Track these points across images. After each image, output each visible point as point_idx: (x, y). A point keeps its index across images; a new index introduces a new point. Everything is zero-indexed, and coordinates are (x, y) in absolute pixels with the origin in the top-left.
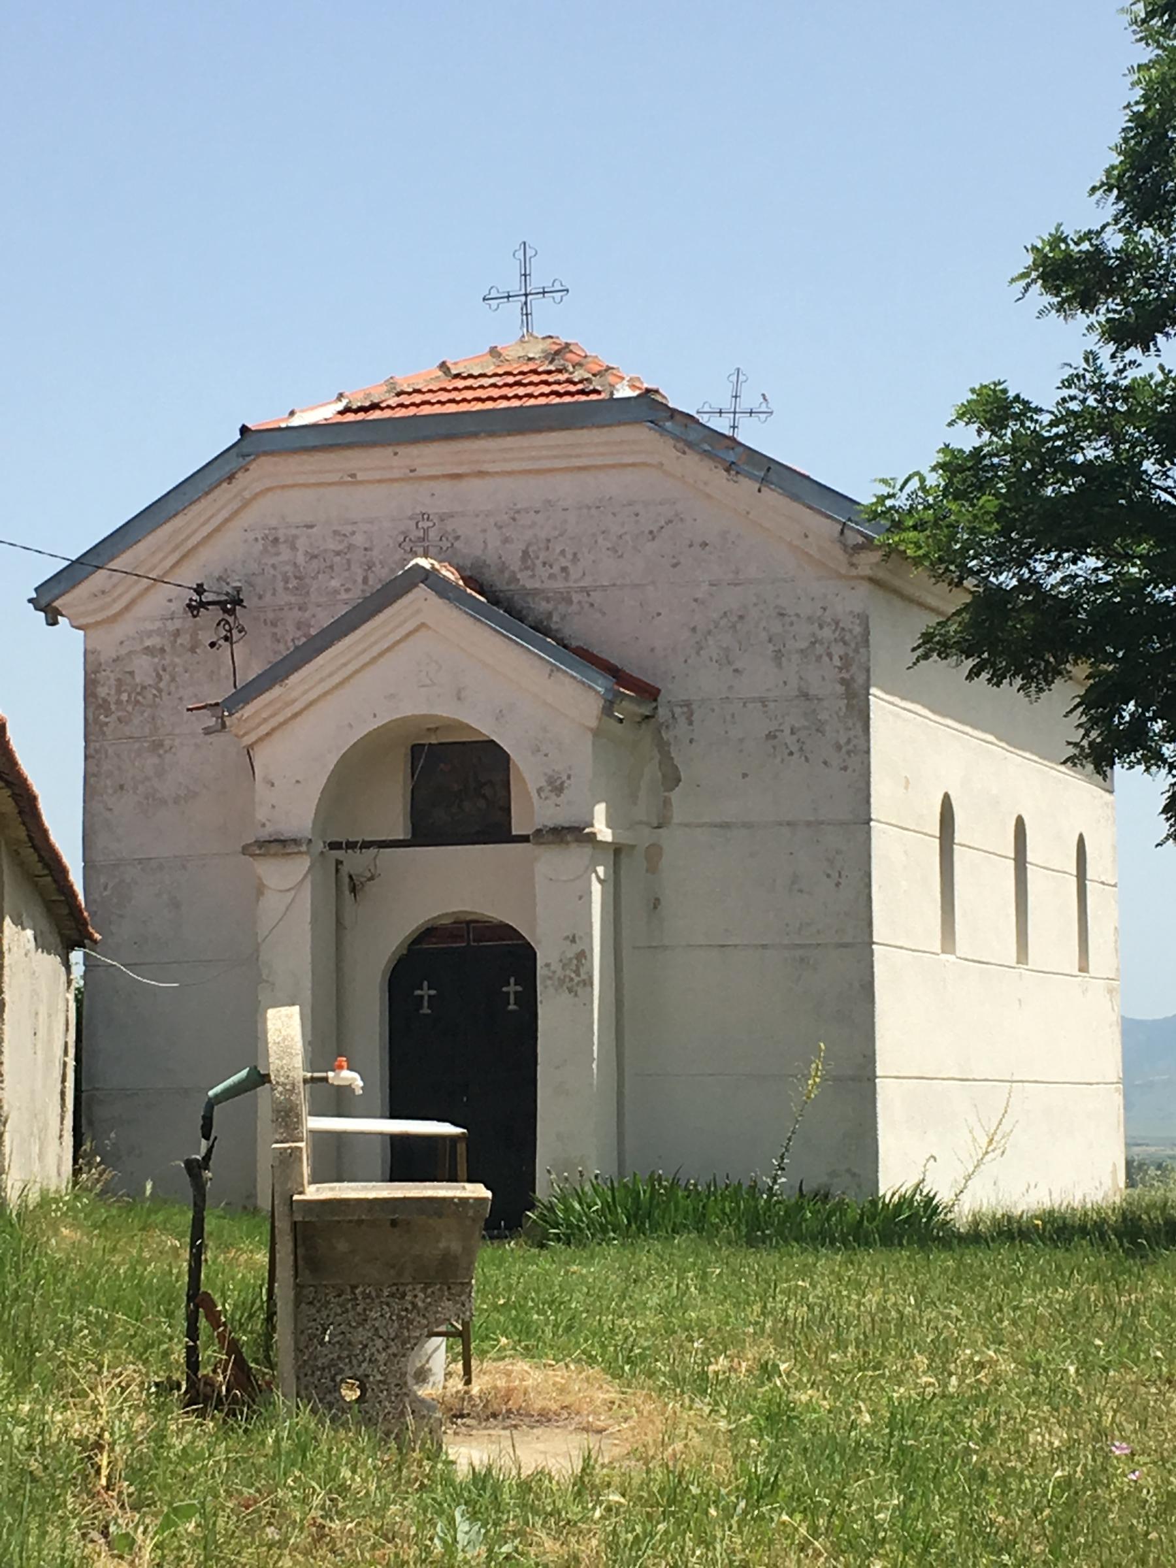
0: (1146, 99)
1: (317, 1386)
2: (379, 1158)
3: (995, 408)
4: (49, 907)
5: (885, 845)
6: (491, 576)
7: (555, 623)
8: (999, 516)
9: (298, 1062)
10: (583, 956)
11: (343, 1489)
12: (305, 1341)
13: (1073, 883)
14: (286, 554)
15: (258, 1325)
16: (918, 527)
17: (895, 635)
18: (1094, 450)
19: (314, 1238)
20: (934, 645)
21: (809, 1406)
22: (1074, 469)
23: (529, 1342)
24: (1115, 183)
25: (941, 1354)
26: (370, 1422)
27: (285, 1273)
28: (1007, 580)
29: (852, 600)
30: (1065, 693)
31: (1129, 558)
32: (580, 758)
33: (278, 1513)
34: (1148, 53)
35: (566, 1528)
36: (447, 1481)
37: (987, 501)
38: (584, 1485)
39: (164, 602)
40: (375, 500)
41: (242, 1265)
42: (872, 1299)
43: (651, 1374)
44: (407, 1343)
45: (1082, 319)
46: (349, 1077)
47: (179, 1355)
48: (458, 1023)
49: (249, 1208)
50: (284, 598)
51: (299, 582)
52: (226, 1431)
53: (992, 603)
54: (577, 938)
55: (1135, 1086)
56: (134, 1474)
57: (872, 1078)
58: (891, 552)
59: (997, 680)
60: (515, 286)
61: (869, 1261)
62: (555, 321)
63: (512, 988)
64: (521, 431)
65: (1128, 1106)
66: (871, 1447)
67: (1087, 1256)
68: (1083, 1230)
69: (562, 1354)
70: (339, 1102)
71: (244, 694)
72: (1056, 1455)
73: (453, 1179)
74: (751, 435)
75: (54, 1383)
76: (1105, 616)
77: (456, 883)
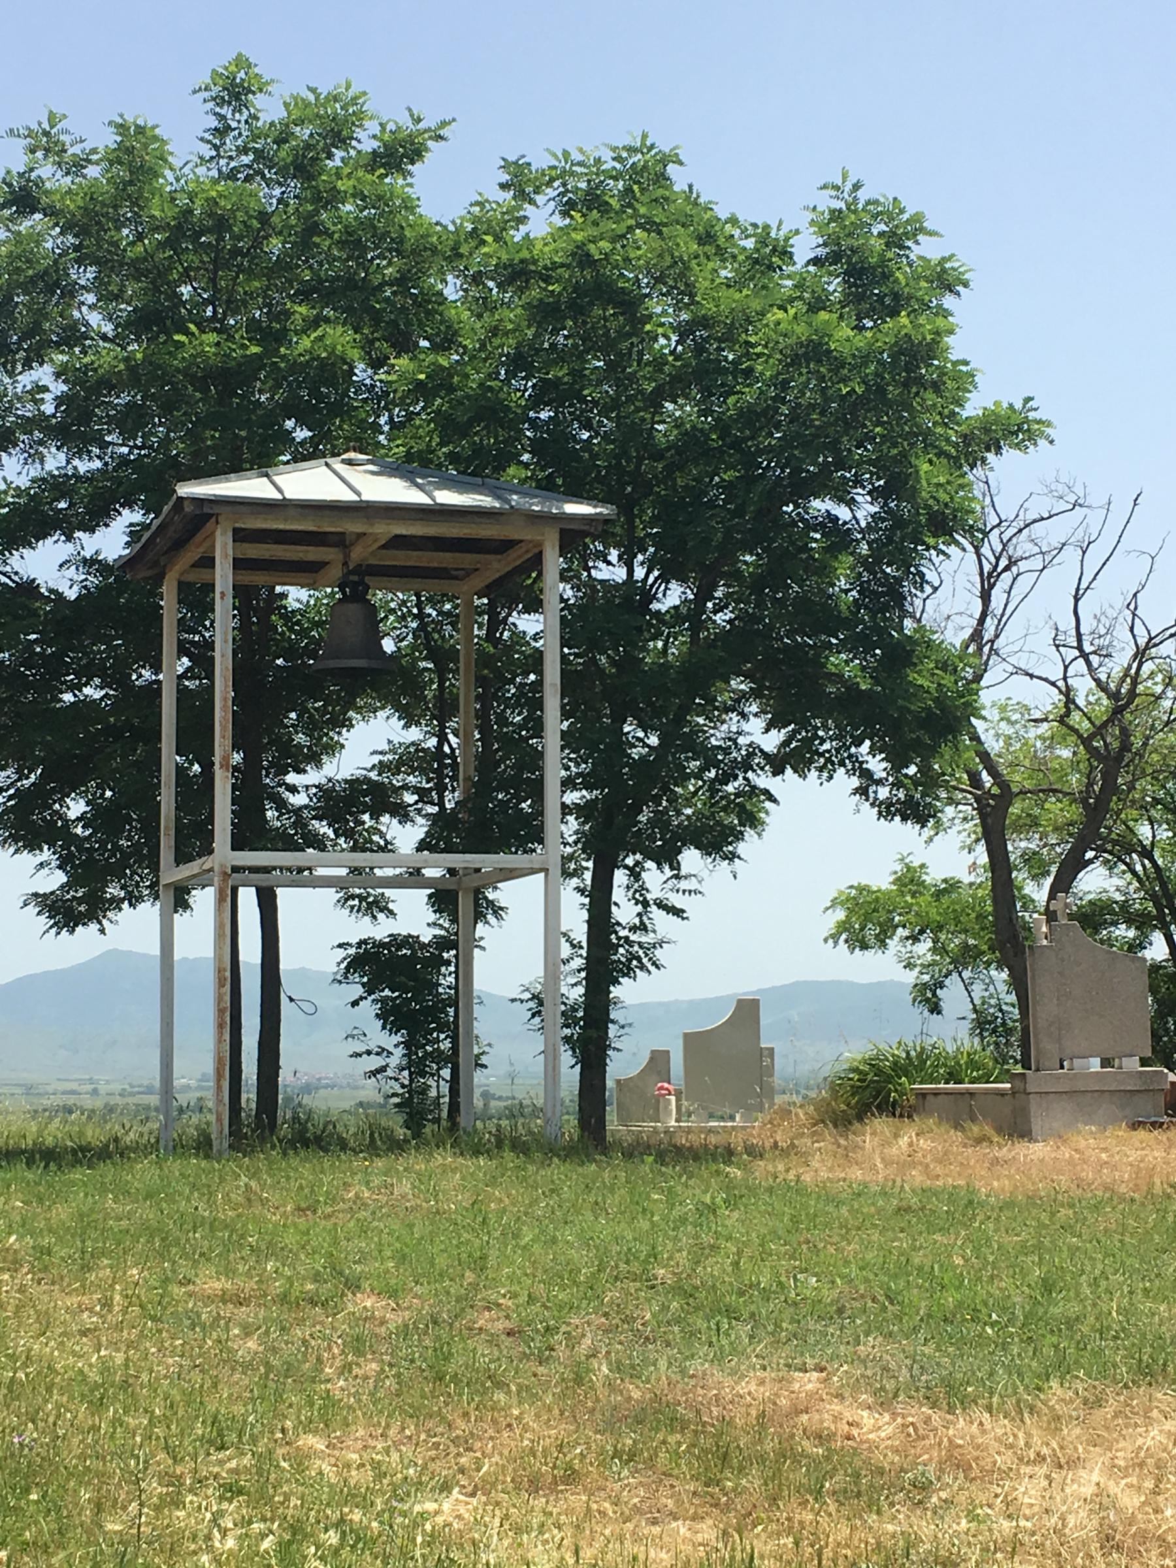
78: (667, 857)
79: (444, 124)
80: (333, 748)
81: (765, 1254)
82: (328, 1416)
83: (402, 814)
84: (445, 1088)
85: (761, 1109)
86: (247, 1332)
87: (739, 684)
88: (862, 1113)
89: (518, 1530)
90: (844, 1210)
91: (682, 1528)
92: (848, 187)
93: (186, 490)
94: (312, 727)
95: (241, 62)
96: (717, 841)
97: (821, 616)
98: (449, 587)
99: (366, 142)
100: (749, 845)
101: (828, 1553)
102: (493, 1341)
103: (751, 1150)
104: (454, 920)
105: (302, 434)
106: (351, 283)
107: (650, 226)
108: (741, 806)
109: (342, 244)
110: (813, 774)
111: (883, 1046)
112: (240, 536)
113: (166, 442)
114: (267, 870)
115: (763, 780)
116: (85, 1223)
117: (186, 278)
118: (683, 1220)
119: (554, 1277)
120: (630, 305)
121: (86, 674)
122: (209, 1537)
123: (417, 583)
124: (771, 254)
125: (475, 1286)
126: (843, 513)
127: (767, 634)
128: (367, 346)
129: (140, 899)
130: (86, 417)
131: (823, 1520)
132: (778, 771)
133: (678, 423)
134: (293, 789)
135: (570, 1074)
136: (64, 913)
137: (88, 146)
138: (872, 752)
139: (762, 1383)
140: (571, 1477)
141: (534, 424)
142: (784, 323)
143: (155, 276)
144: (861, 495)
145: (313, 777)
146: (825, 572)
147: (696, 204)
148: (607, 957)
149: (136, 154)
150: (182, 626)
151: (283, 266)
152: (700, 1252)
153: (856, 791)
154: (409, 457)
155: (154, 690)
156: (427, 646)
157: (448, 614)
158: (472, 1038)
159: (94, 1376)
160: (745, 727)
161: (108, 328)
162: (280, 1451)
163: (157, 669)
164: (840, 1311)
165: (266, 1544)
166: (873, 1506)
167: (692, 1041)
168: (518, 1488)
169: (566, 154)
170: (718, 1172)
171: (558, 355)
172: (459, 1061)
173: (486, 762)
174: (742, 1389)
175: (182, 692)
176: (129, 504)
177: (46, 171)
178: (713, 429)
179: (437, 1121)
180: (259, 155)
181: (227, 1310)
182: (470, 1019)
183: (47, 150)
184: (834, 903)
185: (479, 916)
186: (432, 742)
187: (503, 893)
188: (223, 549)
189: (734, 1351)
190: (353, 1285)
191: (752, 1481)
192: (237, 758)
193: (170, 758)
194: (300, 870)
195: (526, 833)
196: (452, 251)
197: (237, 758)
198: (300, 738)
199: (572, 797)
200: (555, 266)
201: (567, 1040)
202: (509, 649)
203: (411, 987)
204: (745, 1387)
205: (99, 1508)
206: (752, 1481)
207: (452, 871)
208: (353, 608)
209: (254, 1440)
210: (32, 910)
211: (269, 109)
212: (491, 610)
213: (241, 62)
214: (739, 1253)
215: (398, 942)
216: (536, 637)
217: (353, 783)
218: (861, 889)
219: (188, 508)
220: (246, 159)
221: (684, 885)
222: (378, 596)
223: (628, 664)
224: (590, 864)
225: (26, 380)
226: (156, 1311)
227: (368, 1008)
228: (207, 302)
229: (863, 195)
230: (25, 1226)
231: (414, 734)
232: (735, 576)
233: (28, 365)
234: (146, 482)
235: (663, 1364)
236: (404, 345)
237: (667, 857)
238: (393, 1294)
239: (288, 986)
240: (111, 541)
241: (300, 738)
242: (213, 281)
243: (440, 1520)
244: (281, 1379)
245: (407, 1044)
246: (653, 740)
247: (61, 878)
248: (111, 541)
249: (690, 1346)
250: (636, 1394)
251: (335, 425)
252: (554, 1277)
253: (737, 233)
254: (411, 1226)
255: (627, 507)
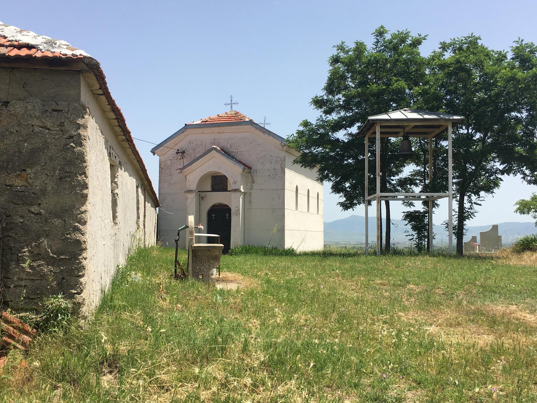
0: (331, 76)
1: (196, 275)
2: (206, 240)
3: (306, 124)
4: (153, 200)
5: (287, 193)
6: (225, 149)
7: (235, 157)
8: (306, 141)
9: (193, 224)
10: (239, 210)
11: (199, 291)
12: (194, 268)
13: (316, 200)
14: (192, 145)
15: (186, 266)
16: (293, 142)
17: (289, 160)
18: (322, 131)
19: (195, 252)
20: (295, 162)
21: (273, 280)
22: (318, 134)
23: (229, 269)
24: (326, 89)
25: (294, 272)
26: (204, 281)
27: (190, 258)
28: (307, 151)
29: (283, 154)
30: (316, 169)
31: (327, 148)
32: (239, 178)
33: (189, 295)
34: (331, 68)
35: (235, 298)
36: (216, 290)
37: (304, 139)
38: (238, 291)
39: (173, 152)
40: (206, 137)
41: (183, 257)
42: (284, 264)
43: (248, 275)
44: (210, 269)
45: (320, 110)
46: (201, 227)
47: (173, 270)
48: (219, 220)
49: (184, 248)
50: (192, 152)
51: (194, 149)
52: (181, 282)
53: (304, 155)
54: (238, 207)
55: (326, 233)
56: (166, 288)
57: (284, 230)
58: (289, 146)
59: (305, 167)
60: (230, 102)
61: (283, 258)
62: (236, 108)
63: (227, 215)
64: (229, 126)
65: (324, 236)
66: (283, 286)
67: (317, 257)
68: (317, 254)
69: (234, 272)
70: (199, 231)
71: (185, 167)
72: (312, 288)
73: (218, 243)
74: (267, 127)
75: (154, 274)
76: (323, 157)
77: (218, 198)
78: (477, 193)
79: (426, 36)
80: (401, 171)
81: (502, 280)
82: (405, 309)
83: (416, 185)
84: (426, 243)
85: (499, 249)
86: (386, 291)
87: (494, 155)
88: (523, 250)
89: (448, 334)
90: (520, 271)
91: (485, 336)
92: (520, 41)
93: (370, 118)
94: (396, 167)
95: (382, 27)
96: (488, 189)
97: (515, 139)
98: (426, 136)
99: (409, 42)
100: (496, 190)
101: (521, 344)
102: (440, 295)
103: (497, 257)
104: (428, 207)
105: (394, 105)
106: (405, 72)
107: (474, 54)
108: (494, 182)
109: (403, 64)
110: (511, 175)
111: (529, 236)
112: (381, 127)
113: (366, 109)
114: (387, 197)
115: (499, 176)
116: (352, 268)
117: (370, 74)
118: (482, 272)
119: (453, 283)
120: (468, 72)
121: (349, 158)
122: (381, 331)
123: (420, 136)
124: (502, 57)
125: (435, 284)
126: (519, 115)
127: (500, 143)
128: (409, 85)
129: (361, 203)
130: (349, 104)
131: (519, 337)
132: (503, 174)
133: (479, 97)
134: (393, 180)
135: (455, 241)
136: (346, 206)
137: (349, 48)
138: (526, 169)
139: (502, 307)
140: (459, 324)
141: (446, 100)
142: (505, 72)
143: (363, 74)
144: (524, 111)
145: (397, 177)
146: (515, 129)
147: (483, 48)
148: (463, 215)
149: (360, 48)
150: (369, 147)
151: (390, 70)
152: (486, 279)
153: (522, 178)
154: (418, 108)
155: (363, 160)
156: (422, 149)
157: (426, 142)
158: (432, 232)
159: (355, 298)
160: (495, 164)
161: (353, 86)
162: (395, 315)
163: (364, 156)
164: (521, 293)
165: (393, 334)
166: (531, 334)
167: (482, 234)
168: (447, 326)
169: (454, 39)
170: (490, 262)
171: (452, 84)
172: (429, 237)
173: (435, 174)
174: (498, 308)
175: (369, 161)
176: (358, 122)
177: (342, 54)
178: (487, 98)
179: (425, 250)
180: (385, 46)
181: (382, 287)
182: (432, 228)
183: (341, 50)
184: (517, 204)
185: (434, 206)
186: (423, 169)
187: (439, 201)
188: (378, 130)
189: (495, 300)
190: (408, 283)
191: (502, 328)
192: (381, 174)
193: (367, 174)
194: (394, 197)
195: (445, 188)
196: (428, 63)
197: (381, 174)
198: (394, 169)
199: (454, 181)
200: (451, 63)
201: (454, 233)
202: (440, 149)
203: (419, 222)
204: (499, 308)
205: (358, 324)
206: (502, 328)
207: (427, 197)
208: (405, 141)
209: (389, 312)
210: (339, 206)
211: (388, 37)
212: (436, 141)
213: (382, 27)
214: (496, 279)
215: (416, 212)
216: (447, 146)
217: (405, 179)
218: (523, 200)
219: (371, 122)
220: (382, 48)
221: (480, 199)
222: (411, 139)
223: (467, 151)
224: (459, 195)
225: (337, 97)
226: (367, 286)
227: (409, 227)
228: (374, 79)
229: (524, 43)
230: (340, 268)
231: (419, 168)
232: (493, 131)
233: (337, 94)
234: (361, 117)
235: (479, 302)
236: (417, 85)
237: (477, 193)
238: (417, 285)
239: (392, 221)
240: (354, 130)
241: (394, 169)
242: (375, 74)
243: (430, 331)
244: (394, 301)
245: (418, 234)
246: (474, 168)
247: (345, 199)
248: (354, 130)
249: (485, 298)
250: (473, 308)
251: (401, 102)
252: (453, 283)
253: (493, 54)
254: (420, 271)
255: (467, 117)
